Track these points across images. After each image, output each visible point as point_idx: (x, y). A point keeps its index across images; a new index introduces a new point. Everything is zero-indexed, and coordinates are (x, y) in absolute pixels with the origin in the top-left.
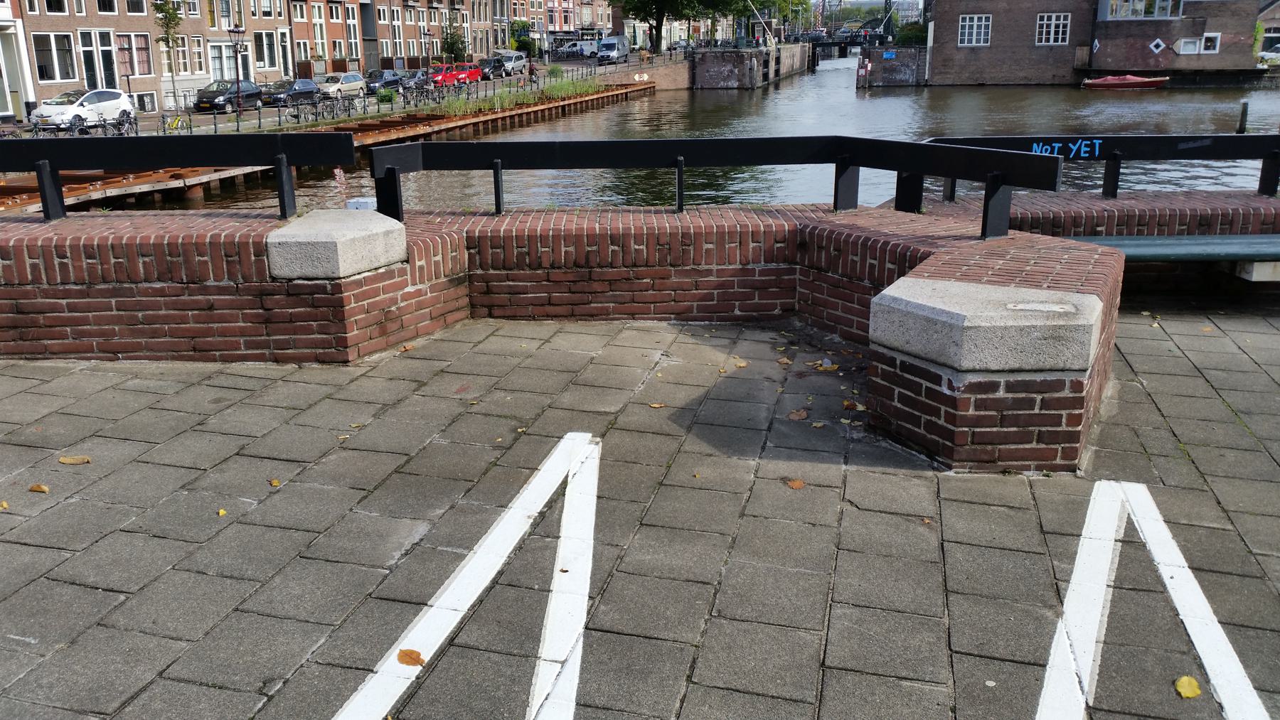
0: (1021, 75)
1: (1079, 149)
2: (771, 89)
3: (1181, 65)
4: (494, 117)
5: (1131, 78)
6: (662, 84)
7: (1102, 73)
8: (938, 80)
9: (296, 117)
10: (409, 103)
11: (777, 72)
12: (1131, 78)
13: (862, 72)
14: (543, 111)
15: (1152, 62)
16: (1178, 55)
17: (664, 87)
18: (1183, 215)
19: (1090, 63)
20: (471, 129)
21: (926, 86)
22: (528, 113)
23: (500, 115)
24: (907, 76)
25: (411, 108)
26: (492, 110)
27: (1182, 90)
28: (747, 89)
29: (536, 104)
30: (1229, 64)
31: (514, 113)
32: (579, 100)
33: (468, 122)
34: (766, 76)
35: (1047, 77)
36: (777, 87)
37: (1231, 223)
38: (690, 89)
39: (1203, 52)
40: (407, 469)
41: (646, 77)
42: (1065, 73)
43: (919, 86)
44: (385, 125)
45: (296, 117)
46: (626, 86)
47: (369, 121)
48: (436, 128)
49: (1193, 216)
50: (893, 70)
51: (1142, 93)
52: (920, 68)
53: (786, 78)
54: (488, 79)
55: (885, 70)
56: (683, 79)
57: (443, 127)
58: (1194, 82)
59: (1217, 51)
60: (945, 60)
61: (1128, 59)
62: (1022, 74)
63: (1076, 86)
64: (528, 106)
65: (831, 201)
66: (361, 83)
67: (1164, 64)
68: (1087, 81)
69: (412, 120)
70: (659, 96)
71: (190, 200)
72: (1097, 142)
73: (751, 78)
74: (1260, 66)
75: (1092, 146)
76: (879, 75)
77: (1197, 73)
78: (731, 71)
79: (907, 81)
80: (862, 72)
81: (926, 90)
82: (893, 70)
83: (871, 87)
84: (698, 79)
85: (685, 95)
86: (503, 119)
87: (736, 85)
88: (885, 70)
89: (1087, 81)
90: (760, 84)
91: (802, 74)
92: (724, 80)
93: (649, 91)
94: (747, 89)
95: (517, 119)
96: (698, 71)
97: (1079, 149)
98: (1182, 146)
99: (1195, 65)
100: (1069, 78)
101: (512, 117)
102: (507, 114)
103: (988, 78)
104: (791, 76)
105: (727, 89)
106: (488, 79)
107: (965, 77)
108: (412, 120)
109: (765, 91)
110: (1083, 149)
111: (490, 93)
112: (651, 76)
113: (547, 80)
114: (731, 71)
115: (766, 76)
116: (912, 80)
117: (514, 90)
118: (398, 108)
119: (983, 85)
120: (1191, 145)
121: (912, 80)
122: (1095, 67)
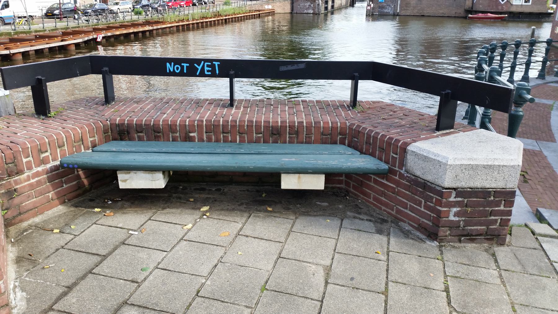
0: (441, 12)
1: (203, 67)
2: (329, 14)
3: (513, 9)
4: (187, 23)
5: (490, 15)
6: (278, 10)
7: (477, 12)
8: (403, 13)
9: (87, 21)
10: (148, 15)
11: (333, 7)
12: (490, 15)
13: (369, 8)
14: (214, 21)
15: (500, 7)
16: (512, 5)
17: (279, 12)
18: (258, 126)
19: (472, 8)
20: (175, 29)
21: (398, 15)
22: (206, 22)
23: (191, 22)
24: (389, 10)
25: (149, 18)
26: (188, 20)
27: (513, 21)
28: (316, 14)
29: (211, 18)
30: (535, 10)
31: (198, 21)
32: (234, 16)
33: (173, 25)
34: (326, 8)
35: (453, 13)
36: (332, 13)
37: (297, 133)
38: (291, 13)
39: (524, 4)
40: (96, 259)
41: (270, 7)
42: (461, 12)
43: (394, 16)
44: (134, 25)
45: (87, 21)
46: (259, 11)
47: (126, 23)
48: (155, 28)
49: (267, 127)
50: (383, 7)
51: (494, 22)
52: (395, 7)
53: (338, 9)
54: (195, 5)
55: (380, 7)
56: (288, 9)
57: (159, 27)
58: (519, 18)
59: (530, 4)
60: (407, 4)
61: (489, 6)
62: (441, 12)
63: (465, 18)
64: (207, 18)
65: (103, 95)
66: (131, 6)
67: (505, 9)
68: (470, 16)
69: (148, 23)
70: (277, 17)
71: (15, 60)
72: (216, 64)
73: (318, 9)
74: (550, 11)
75: (213, 66)
76: (377, 10)
77: (520, 13)
78: (310, 6)
79: (389, 13)
80: (369, 8)
81: (398, 17)
82: (383, 7)
83: (373, 15)
84: (294, 8)
85: (288, 17)
86: (193, 24)
87: (312, 12)
88: (380, 7)
89: (470, 16)
90: (323, 12)
91: (346, 7)
92: (306, 9)
93: (272, 13)
94: (316, 14)
95: (200, 25)
96: (295, 5)
97: (203, 67)
98: (283, 68)
99: (520, 10)
100: (463, 14)
101: (197, 23)
102: (195, 22)
103: (426, 13)
104: (340, 8)
105: (308, 13)
106: (195, 5)
107: (415, 12)
108: (148, 23)
109: (326, 15)
110: (206, 68)
111: (186, 12)
112: (273, 7)
113: (221, 6)
114: (310, 6)
115: (326, 8)
116: (391, 12)
117: (203, 11)
118: (142, 18)
119: (423, 16)
120: (290, 68)
121: (391, 12)
122: (474, 9)
